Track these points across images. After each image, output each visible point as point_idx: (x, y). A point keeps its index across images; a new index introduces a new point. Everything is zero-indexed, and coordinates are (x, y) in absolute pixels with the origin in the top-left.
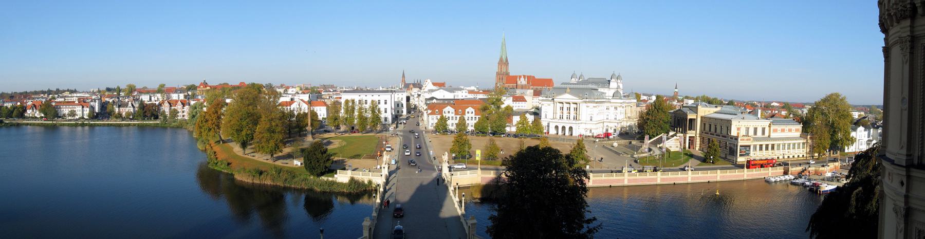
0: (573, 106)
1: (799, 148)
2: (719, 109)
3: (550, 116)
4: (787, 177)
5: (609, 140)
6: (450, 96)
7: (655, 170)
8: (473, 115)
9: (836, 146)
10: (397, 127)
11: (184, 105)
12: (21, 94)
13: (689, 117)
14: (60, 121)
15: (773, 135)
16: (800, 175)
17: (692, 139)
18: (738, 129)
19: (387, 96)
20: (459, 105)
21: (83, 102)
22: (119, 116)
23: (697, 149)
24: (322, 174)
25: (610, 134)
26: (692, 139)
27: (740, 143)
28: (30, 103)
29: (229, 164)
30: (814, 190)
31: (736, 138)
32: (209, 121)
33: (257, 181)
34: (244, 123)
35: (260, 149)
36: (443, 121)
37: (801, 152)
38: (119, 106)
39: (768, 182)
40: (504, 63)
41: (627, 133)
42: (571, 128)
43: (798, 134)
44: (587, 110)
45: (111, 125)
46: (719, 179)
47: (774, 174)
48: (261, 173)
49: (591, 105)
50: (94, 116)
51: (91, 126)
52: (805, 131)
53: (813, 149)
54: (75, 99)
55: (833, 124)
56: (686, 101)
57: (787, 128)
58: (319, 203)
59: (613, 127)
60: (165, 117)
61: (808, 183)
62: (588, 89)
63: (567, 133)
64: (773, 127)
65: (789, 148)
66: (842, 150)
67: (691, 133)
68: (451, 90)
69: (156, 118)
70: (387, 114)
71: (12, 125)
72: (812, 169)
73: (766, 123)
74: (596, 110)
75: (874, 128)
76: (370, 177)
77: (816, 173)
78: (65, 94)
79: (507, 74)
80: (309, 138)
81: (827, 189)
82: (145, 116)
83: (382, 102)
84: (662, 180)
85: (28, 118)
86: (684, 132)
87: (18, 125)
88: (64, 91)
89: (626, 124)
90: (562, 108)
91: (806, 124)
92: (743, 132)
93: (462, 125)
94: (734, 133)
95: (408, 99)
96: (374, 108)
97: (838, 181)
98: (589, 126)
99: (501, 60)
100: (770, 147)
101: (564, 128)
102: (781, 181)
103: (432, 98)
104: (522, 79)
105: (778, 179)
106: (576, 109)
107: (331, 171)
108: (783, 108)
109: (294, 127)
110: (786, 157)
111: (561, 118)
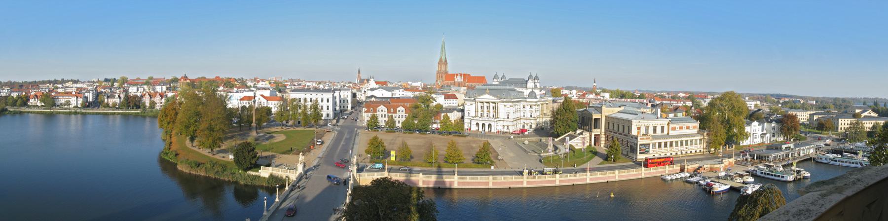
0: (492, 105)
1: (696, 144)
2: (622, 108)
3: (473, 114)
4: (683, 175)
5: (525, 136)
6: (388, 94)
7: (555, 172)
8: (404, 114)
9: (730, 140)
10: (338, 121)
11: (162, 97)
12: (30, 83)
13: (594, 117)
14: (56, 110)
15: (672, 133)
16: (696, 172)
17: (597, 138)
18: (639, 128)
19: (329, 96)
20: (391, 103)
21: (79, 92)
22: (107, 106)
23: (602, 147)
24: (249, 169)
25: (526, 131)
26: (597, 138)
27: (640, 142)
28: (33, 93)
29: (176, 155)
30: (707, 190)
31: (636, 138)
32: (170, 114)
33: (193, 172)
34: (192, 121)
35: (202, 144)
36: (374, 119)
37: (698, 147)
38: (108, 97)
39: (664, 180)
40: (443, 62)
41: (542, 129)
42: (490, 125)
43: (696, 131)
44: (504, 109)
45: (99, 113)
46: (617, 179)
47: (669, 172)
48: (198, 165)
49: (508, 104)
50: (87, 105)
51: (83, 114)
52: (702, 128)
53: (710, 144)
54: (74, 90)
55: (728, 120)
56: (602, 94)
57: (685, 125)
58: (248, 194)
59: (530, 125)
60: (145, 106)
61: (702, 182)
62: (508, 89)
63: (487, 130)
64: (671, 126)
65: (687, 145)
66: (737, 143)
67: (596, 132)
68: (389, 90)
69: (138, 107)
70: (327, 111)
71: (15, 113)
72: (707, 166)
73: (665, 122)
74: (513, 109)
75: (768, 122)
76: (288, 174)
77: (712, 170)
78: (67, 84)
79: (446, 72)
80: (254, 134)
81: (720, 189)
82: (129, 106)
83: (325, 100)
84: (560, 181)
85: (29, 107)
86: (590, 131)
87: (21, 113)
88: (68, 81)
89: (541, 120)
90: (482, 107)
91: (704, 121)
92: (643, 131)
93: (391, 123)
94: (634, 132)
95: (354, 95)
96: (315, 107)
97: (732, 179)
98: (506, 123)
99: (441, 60)
100: (668, 144)
101: (483, 125)
102: (676, 179)
103: (372, 96)
104: (459, 77)
105: (674, 177)
106: (495, 108)
107: (257, 167)
108: (688, 98)
109: (244, 120)
110: (684, 152)
111: (482, 115)
